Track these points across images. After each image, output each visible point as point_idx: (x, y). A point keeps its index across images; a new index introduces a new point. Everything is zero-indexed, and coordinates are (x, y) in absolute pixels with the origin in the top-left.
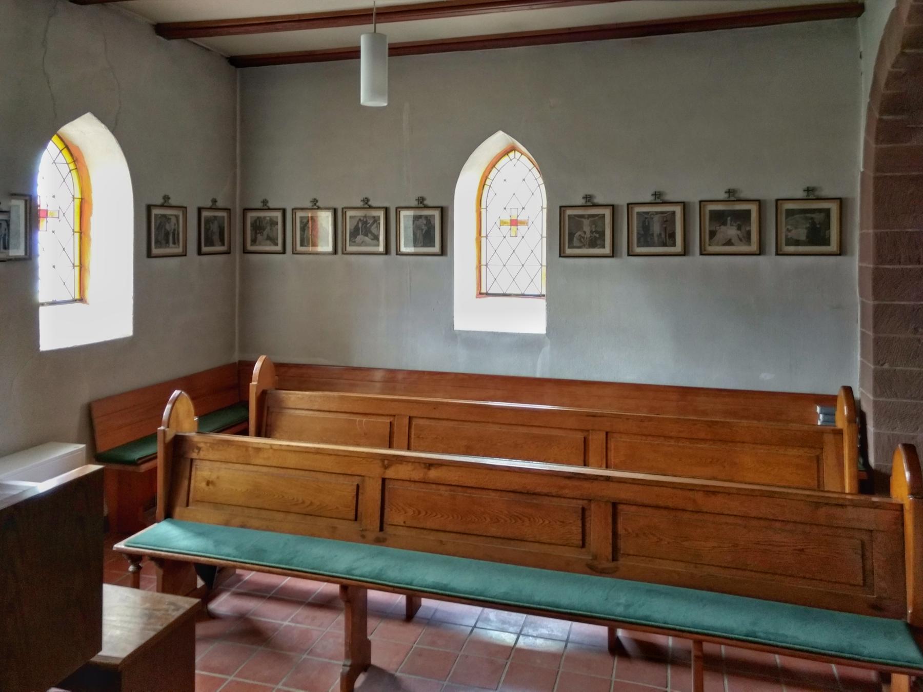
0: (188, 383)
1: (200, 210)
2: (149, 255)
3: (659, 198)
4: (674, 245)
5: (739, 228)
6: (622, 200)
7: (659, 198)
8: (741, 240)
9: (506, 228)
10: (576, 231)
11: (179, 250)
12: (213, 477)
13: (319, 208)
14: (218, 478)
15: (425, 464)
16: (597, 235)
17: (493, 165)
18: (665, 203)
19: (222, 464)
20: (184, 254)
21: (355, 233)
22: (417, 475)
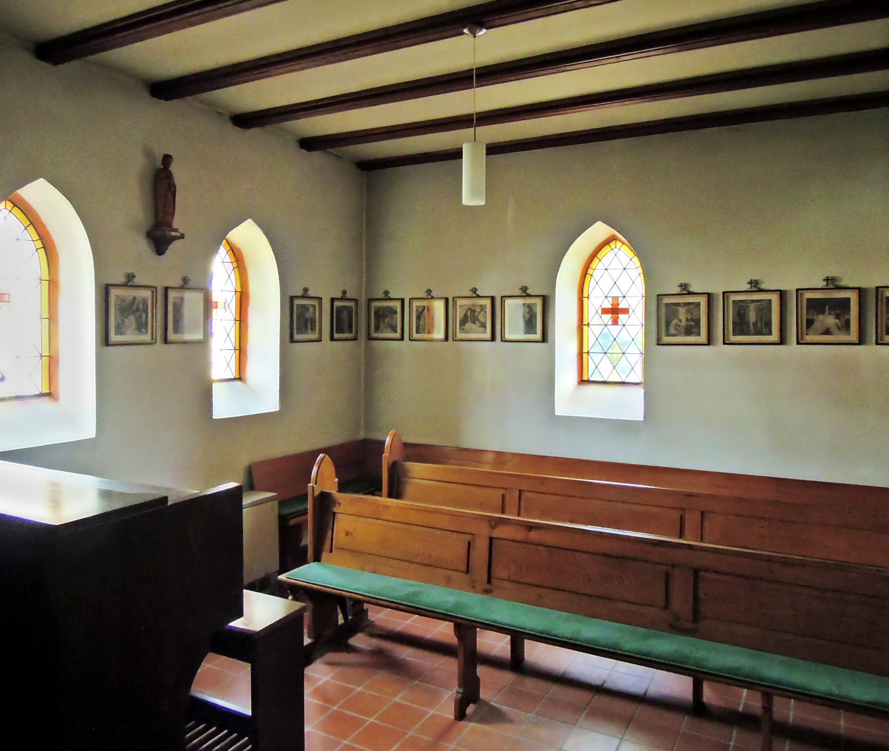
0: (326, 451)
1: (333, 300)
2: (292, 340)
3: (755, 286)
4: (770, 333)
5: (838, 317)
6: (717, 289)
7: (755, 286)
8: (839, 329)
9: (608, 317)
10: (675, 319)
11: (315, 336)
12: (351, 530)
13: (433, 298)
14: (355, 529)
15: (526, 526)
16: (693, 323)
17: (594, 255)
18: (761, 291)
19: (353, 516)
20: (319, 340)
21: (464, 322)
22: (519, 535)
